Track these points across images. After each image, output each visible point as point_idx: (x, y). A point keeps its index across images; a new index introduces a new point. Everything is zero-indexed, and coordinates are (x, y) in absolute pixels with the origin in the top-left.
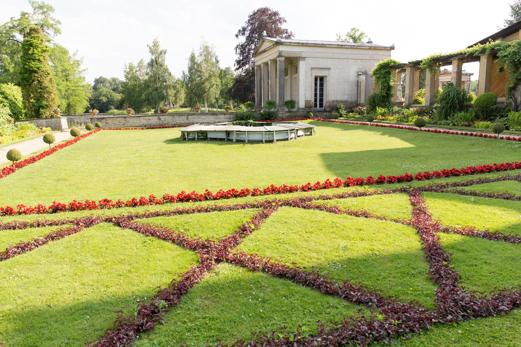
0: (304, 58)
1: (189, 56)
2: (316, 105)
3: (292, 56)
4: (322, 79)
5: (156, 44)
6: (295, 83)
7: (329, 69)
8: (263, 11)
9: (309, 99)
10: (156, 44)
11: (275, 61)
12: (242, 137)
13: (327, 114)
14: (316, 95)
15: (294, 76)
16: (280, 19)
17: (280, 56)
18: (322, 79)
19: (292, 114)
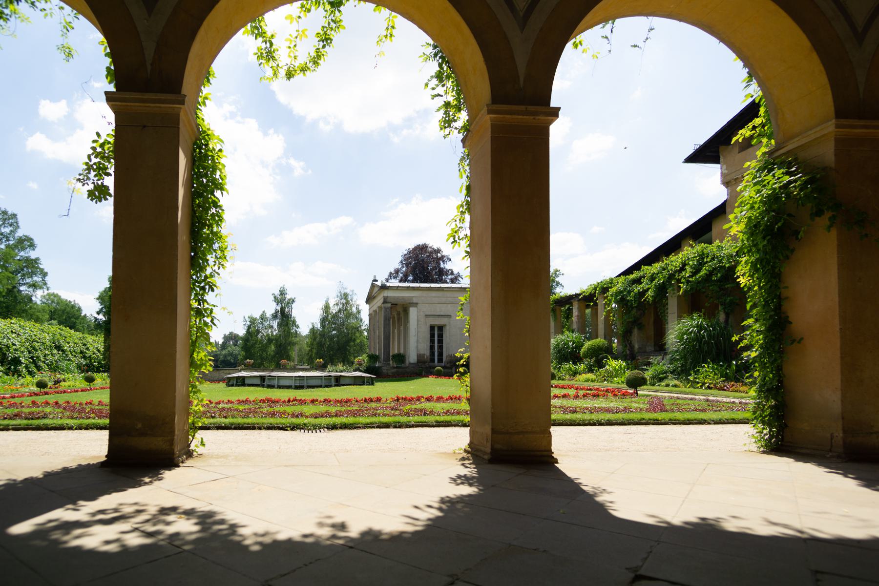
0: (415, 305)
1: (322, 304)
2: (432, 360)
4: (441, 328)
5: (283, 293)
7: (449, 316)
8: (422, 248)
9: (422, 352)
10: (283, 293)
16: (443, 257)
17: (385, 302)
18: (441, 328)
19: (400, 370)
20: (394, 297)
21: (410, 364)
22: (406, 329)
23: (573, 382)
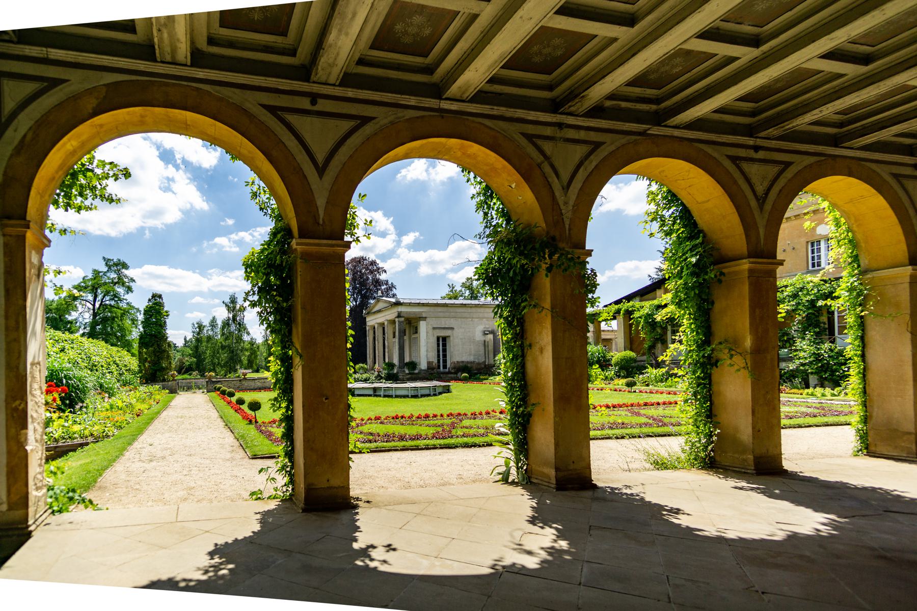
0: (425, 319)
2: (439, 366)
4: (444, 339)
6: (415, 342)
7: (452, 328)
11: (393, 322)
12: (390, 393)
14: (439, 356)
15: (413, 336)
16: (379, 269)
17: (399, 316)
20: (407, 312)
21: (421, 370)
22: (417, 340)
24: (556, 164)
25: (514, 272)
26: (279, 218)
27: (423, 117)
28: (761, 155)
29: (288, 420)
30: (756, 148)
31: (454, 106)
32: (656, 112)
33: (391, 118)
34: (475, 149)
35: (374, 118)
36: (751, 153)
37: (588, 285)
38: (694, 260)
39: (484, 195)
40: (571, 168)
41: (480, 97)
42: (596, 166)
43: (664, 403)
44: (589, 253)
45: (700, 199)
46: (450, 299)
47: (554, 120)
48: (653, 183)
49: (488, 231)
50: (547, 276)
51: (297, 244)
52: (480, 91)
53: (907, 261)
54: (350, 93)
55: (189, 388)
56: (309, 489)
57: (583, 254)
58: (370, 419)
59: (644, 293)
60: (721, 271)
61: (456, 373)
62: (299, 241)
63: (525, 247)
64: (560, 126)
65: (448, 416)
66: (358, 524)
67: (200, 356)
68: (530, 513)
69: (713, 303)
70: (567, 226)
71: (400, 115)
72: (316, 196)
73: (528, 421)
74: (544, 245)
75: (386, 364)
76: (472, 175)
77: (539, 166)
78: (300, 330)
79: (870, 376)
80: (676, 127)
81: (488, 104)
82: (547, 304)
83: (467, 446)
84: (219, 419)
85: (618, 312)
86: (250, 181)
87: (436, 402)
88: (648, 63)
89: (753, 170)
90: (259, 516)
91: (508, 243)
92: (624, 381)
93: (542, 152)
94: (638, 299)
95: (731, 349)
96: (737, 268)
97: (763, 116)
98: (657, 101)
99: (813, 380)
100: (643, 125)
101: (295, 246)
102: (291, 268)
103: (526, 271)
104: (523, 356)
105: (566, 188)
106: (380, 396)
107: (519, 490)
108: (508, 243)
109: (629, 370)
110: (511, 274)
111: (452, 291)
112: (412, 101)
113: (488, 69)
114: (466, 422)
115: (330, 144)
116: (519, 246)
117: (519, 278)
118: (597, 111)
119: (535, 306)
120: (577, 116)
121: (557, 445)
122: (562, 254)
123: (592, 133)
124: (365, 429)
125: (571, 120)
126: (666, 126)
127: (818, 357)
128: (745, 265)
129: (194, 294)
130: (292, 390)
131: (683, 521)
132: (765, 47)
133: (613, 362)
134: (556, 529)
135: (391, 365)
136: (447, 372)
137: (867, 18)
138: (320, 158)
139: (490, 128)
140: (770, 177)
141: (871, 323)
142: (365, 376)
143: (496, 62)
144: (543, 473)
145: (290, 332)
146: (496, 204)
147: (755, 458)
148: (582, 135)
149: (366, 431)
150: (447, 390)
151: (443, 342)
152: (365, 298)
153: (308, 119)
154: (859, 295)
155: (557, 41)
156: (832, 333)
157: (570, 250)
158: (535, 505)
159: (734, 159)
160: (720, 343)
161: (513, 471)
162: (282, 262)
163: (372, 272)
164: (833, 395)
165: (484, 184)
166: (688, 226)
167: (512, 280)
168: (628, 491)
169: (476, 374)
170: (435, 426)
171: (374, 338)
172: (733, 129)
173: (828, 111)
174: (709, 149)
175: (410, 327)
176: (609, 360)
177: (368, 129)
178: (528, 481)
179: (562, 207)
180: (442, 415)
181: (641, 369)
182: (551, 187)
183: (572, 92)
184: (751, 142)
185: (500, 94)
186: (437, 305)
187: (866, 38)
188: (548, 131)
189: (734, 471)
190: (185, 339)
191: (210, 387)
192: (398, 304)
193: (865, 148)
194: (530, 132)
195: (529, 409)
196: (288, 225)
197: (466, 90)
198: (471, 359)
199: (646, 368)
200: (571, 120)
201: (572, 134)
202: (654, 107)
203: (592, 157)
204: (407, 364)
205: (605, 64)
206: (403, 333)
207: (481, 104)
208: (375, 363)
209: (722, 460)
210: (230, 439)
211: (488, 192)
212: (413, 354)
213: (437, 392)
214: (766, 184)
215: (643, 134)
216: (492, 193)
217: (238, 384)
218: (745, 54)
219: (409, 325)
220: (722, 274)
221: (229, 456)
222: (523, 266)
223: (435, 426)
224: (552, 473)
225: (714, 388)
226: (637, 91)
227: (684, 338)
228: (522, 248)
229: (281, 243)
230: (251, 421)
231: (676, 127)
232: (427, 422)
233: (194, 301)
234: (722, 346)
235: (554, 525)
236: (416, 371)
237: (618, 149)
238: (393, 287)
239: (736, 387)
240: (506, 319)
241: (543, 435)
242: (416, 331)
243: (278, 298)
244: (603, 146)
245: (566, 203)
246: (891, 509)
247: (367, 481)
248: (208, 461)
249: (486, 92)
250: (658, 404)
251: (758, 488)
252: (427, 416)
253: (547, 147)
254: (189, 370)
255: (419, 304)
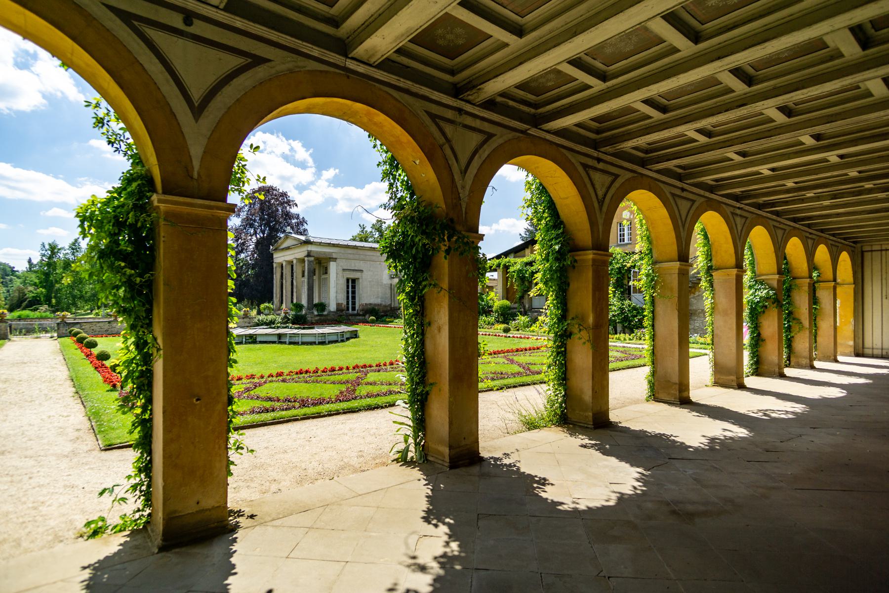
0: (335, 259)
3: (322, 256)
4: (354, 281)
6: (324, 283)
7: (361, 271)
11: (302, 261)
12: (296, 339)
13: (360, 317)
15: (324, 276)
17: (309, 255)
20: (317, 252)
21: (330, 312)
22: (327, 280)
23: (492, 330)
24: (456, 148)
25: (417, 249)
26: (137, 160)
27: (326, 72)
28: (601, 166)
29: (145, 424)
30: (599, 160)
31: (361, 69)
32: (534, 115)
33: (290, 65)
34: (382, 118)
35: (269, 61)
36: (594, 163)
37: (479, 269)
38: (557, 247)
39: (391, 165)
40: (468, 154)
41: (387, 65)
42: (488, 156)
43: (530, 349)
44: (481, 237)
45: (563, 195)
46: (361, 241)
47: (455, 105)
48: (530, 175)
49: (392, 203)
50: (445, 258)
51: (159, 201)
52: (387, 59)
53: (676, 256)
54: (239, 23)
55: (29, 331)
56: (169, 519)
57: (476, 238)
58: (271, 376)
59: (517, 251)
60: (574, 254)
61: (364, 315)
62: (163, 197)
63: (427, 226)
64: (460, 111)
65: (354, 368)
66: (233, 560)
67: (52, 286)
68: (424, 505)
69: (569, 284)
70: (464, 209)
71: (300, 64)
72: (189, 142)
73: (426, 398)
74: (444, 227)
75: (294, 305)
76: (378, 143)
77: (441, 147)
78: (162, 311)
79: (656, 340)
80: (548, 132)
81: (396, 75)
82: (445, 285)
83: (370, 408)
84: (69, 383)
85: (499, 265)
86: (94, 102)
87: (343, 349)
88: (531, 73)
89: (597, 177)
90: (87, 574)
91: (412, 220)
92: (503, 326)
93: (444, 134)
94: (512, 255)
95: (580, 325)
96: (585, 257)
97: (603, 136)
98: (536, 106)
99: (619, 327)
100: (525, 122)
101: (156, 204)
102: (152, 233)
103: (427, 250)
104: (423, 334)
105: (464, 172)
106: (285, 343)
107: (416, 473)
108: (412, 220)
109: (506, 316)
110: (414, 251)
111: (362, 231)
112: (316, 52)
113: (395, 41)
114: (372, 377)
115: (211, 80)
116: (422, 225)
117: (421, 255)
118: (490, 104)
119: (434, 285)
120: (474, 104)
121: (451, 423)
122: (459, 238)
123: (486, 124)
124: (262, 391)
125: (468, 108)
126: (540, 129)
127: (622, 309)
128: (590, 255)
129: (51, 205)
130: (150, 385)
131: (549, 494)
132: (610, 83)
133: (494, 309)
134: (449, 525)
135: (299, 307)
136: (356, 314)
137: (669, 81)
138: (196, 95)
139: (396, 100)
140: (607, 184)
141: (658, 302)
142: (270, 317)
143: (402, 35)
144: (439, 451)
145: (149, 312)
146: (401, 175)
147: (594, 415)
148: (477, 124)
149: (263, 395)
150: (354, 335)
151: (352, 284)
152: (274, 231)
153: (181, 42)
154: (652, 280)
155: (459, 30)
156: (629, 293)
157: (466, 234)
158: (430, 493)
159: (585, 166)
160: (573, 319)
161: (412, 448)
162: (137, 221)
163: (282, 204)
164: (630, 339)
165: (389, 155)
166: (547, 203)
167: (415, 257)
168: (506, 461)
169: (383, 316)
170: (341, 383)
171: (282, 274)
172: (585, 142)
173: (642, 141)
174: (568, 154)
175: (320, 266)
176: (491, 307)
177: (261, 72)
178: (423, 460)
179: (460, 191)
180: (348, 368)
181: (513, 316)
182: (451, 170)
183: (470, 82)
184: (595, 154)
185: (408, 67)
186: (347, 247)
187: (670, 95)
188: (449, 114)
189: (581, 427)
190: (30, 261)
191: (63, 330)
192: (307, 242)
193: (658, 172)
194: (433, 112)
195: (427, 389)
196: (149, 171)
197: (373, 55)
198: (378, 301)
199: (517, 315)
200: (468, 108)
201: (469, 121)
202: (533, 111)
203: (485, 146)
204: (316, 305)
205: (497, 64)
206: (312, 273)
207: (389, 73)
208: (282, 303)
209: (572, 416)
210: (77, 416)
211: (394, 163)
212: (323, 295)
213: (345, 337)
214: (604, 190)
215: (524, 132)
216: (398, 164)
217: (107, 326)
218: (597, 85)
219: (319, 265)
220: (576, 261)
221: (69, 447)
222: (424, 245)
223: (341, 383)
224: (446, 450)
225: (568, 355)
226: (521, 93)
227: (548, 312)
228: (424, 227)
229: (140, 194)
230: (114, 386)
231: (548, 132)
232: (332, 378)
233: (50, 213)
234: (574, 322)
235: (447, 520)
236: (325, 313)
237: (506, 142)
238: (303, 222)
239: (582, 356)
240: (408, 294)
241: (439, 413)
242: (326, 272)
243: (129, 271)
244: (494, 138)
245: (463, 187)
246: (673, 456)
247: (257, 472)
248: (32, 462)
249: (393, 62)
250: (526, 350)
251: (596, 445)
252: (333, 369)
253: (448, 129)
254: (33, 304)
255: (329, 245)
